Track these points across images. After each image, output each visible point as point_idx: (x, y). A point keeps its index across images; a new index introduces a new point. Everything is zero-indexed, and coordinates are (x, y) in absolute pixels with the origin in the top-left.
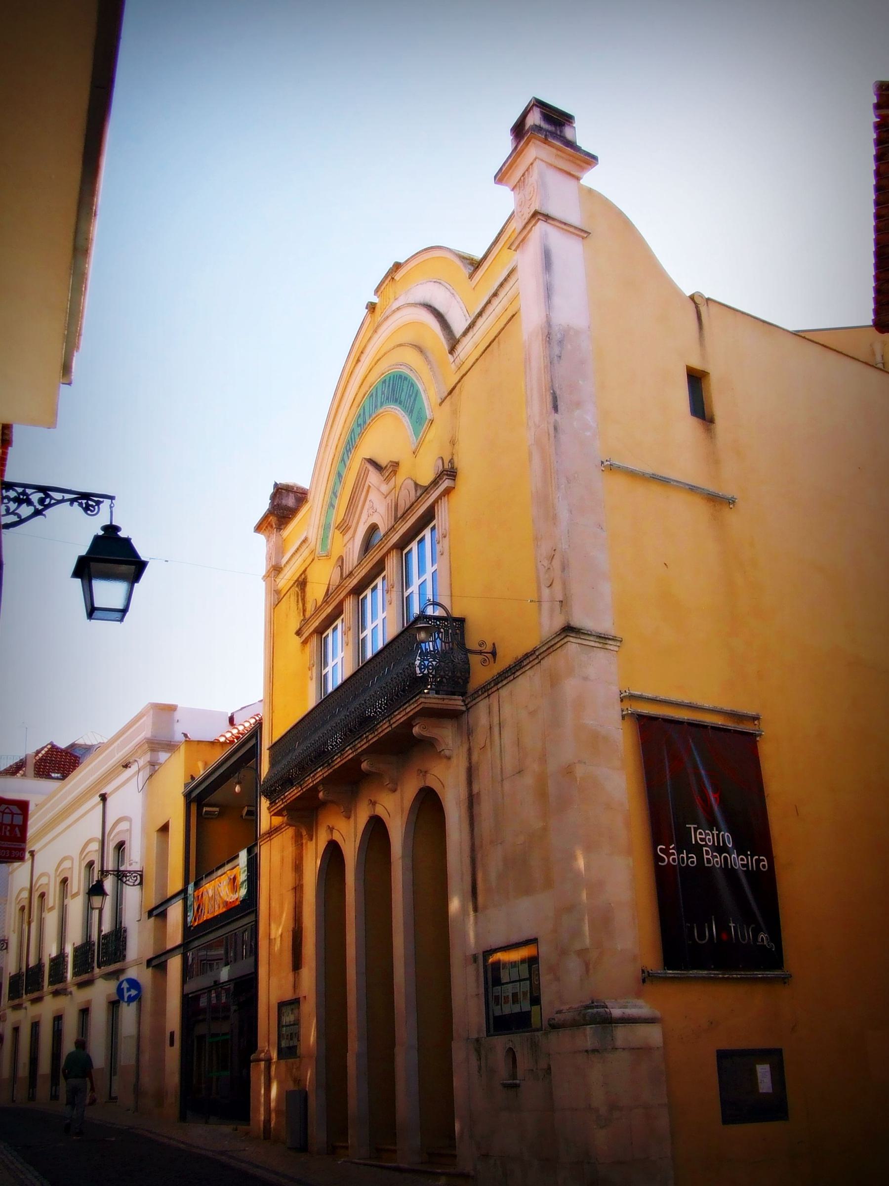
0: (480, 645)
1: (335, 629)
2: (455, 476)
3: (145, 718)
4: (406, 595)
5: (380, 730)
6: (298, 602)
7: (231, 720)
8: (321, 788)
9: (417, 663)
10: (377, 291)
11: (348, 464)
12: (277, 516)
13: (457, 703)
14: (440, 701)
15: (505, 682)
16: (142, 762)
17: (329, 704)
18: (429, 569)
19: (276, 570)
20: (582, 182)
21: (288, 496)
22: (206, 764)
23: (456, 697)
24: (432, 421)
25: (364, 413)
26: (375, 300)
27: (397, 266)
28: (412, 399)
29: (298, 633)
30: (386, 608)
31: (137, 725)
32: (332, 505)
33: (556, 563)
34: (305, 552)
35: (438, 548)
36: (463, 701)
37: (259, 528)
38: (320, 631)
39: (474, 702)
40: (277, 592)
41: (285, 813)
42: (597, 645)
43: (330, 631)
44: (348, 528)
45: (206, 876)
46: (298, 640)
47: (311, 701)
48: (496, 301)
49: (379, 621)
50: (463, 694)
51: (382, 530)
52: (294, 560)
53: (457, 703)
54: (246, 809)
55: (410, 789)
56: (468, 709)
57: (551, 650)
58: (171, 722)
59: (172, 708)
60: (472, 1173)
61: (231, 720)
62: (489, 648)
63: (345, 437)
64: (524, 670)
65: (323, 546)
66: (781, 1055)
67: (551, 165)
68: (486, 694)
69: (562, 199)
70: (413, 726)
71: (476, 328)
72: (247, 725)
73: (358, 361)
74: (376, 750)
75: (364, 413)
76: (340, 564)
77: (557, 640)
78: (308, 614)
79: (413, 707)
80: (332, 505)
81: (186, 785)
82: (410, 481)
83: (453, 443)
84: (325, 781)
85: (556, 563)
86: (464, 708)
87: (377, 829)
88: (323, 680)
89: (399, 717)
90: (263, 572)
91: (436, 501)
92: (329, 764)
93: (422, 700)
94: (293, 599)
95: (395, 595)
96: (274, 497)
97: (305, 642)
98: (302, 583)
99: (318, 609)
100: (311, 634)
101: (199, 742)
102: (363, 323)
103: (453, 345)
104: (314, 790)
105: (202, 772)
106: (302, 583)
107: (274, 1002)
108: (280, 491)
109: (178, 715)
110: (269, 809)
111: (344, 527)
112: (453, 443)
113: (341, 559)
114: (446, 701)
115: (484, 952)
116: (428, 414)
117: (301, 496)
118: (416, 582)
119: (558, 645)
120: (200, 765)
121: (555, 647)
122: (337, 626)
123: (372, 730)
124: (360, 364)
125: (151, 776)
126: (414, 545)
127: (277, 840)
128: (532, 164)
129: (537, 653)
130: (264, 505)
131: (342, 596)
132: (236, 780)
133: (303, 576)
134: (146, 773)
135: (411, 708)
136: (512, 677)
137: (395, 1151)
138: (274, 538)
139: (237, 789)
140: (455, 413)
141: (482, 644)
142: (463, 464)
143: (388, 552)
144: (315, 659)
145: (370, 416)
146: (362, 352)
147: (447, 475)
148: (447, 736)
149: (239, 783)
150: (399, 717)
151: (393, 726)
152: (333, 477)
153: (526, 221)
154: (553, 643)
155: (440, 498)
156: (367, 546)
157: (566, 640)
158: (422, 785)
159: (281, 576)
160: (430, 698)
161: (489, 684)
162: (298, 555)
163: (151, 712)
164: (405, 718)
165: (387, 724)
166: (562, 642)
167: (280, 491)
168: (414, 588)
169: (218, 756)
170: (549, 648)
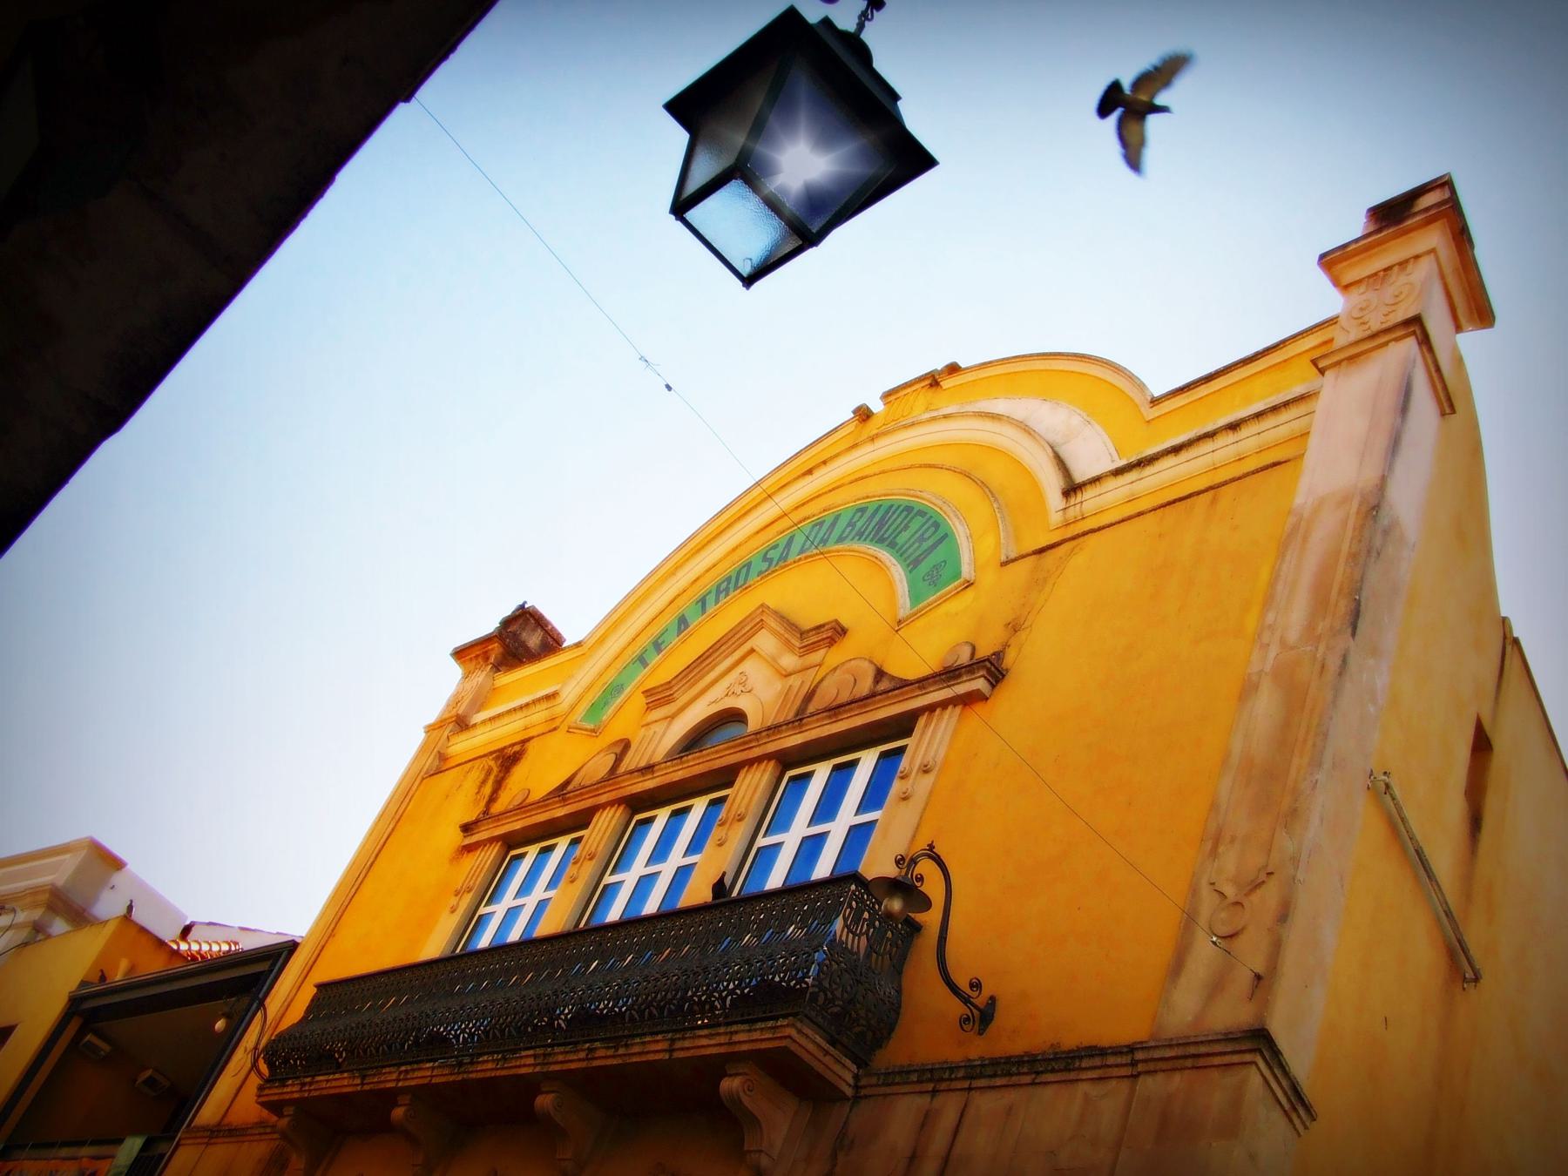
0: (972, 986)
2: (998, 681)
3: (67, 856)
4: (762, 841)
5: (636, 1049)
6: (484, 782)
7: (186, 931)
8: (406, 1099)
10: (887, 396)
11: (711, 609)
12: (506, 647)
13: (843, 1073)
14: (820, 1055)
15: (998, 1082)
16: (22, 917)
17: (460, 964)
18: (539, 892)
19: (460, 723)
20: (1459, 336)
21: (534, 630)
22: (132, 968)
23: (848, 1063)
24: (969, 584)
25: (833, 524)
26: (877, 406)
27: (953, 369)
28: (926, 545)
29: (467, 828)
30: (562, 884)
31: (54, 859)
32: (642, 660)
33: (1269, 896)
34: (538, 716)
35: (571, 870)
36: (856, 1077)
37: (460, 654)
38: (512, 843)
39: (888, 1090)
40: (443, 757)
41: (289, 1110)
42: (1284, 1101)
44: (668, 700)
45: (35, 1146)
46: (455, 838)
47: (433, 947)
48: (1170, 461)
50: (861, 1063)
51: (754, 724)
52: (506, 720)
53: (843, 1073)
54: (149, 1073)
56: (857, 1098)
57: (1189, 1063)
58: (102, 883)
59: (117, 864)
61: (186, 931)
62: (980, 1001)
63: (727, 568)
64: (1072, 1076)
65: (561, 732)
67: (1442, 277)
68: (930, 1086)
70: (725, 1075)
71: (1149, 470)
72: (215, 948)
73: (810, 472)
74: (586, 1084)
75: (833, 524)
76: (618, 750)
77: (1218, 1048)
78: (497, 808)
79: (756, 1035)
80: (642, 660)
81: (83, 984)
82: (866, 664)
83: (1014, 627)
84: (426, 1094)
85: (1269, 896)
86: (849, 1092)
88: (474, 922)
89: (705, 1042)
90: (432, 716)
91: (931, 708)
92: (460, 1064)
93: (792, 1032)
94: (476, 775)
95: (588, 870)
96: (507, 623)
97: (468, 849)
98: (508, 759)
99: (522, 808)
100: (492, 840)
101: (143, 930)
102: (835, 430)
103: (1072, 489)
104: (389, 1097)
105: (118, 977)
106: (508, 759)
108: (525, 617)
109: (118, 879)
110: (261, 1088)
111: (658, 697)
112: (1014, 627)
113: (626, 745)
114: (827, 1059)
116: (966, 571)
117: (552, 643)
118: (508, 900)
119: (1217, 1061)
120: (124, 965)
121: (1202, 1062)
123: (615, 1042)
124: (809, 478)
125: (25, 944)
126: (532, 851)
128: (1417, 257)
129: (1139, 1055)
130: (488, 624)
131: (603, 799)
132: (226, 1009)
133: (517, 748)
134: (23, 935)
135: (747, 1038)
136: (1028, 1079)
138: (481, 677)
139: (220, 1025)
140: (1038, 583)
142: (1026, 662)
143: (759, 760)
144: (480, 880)
145: (802, 551)
146: (824, 462)
147: (989, 670)
149: (228, 1016)
150: (705, 1042)
151: (677, 1055)
152: (669, 619)
153: (1389, 324)
154: (1203, 1049)
155: (944, 705)
156: (695, 740)
157: (1248, 1057)
159: (463, 736)
160: (804, 1039)
161: (952, 1069)
162: (520, 715)
163: (83, 853)
164: (722, 1050)
165: (664, 1045)
166: (1235, 1058)
167: (525, 617)
168: (499, 910)
169: (154, 965)
170: (1186, 1057)
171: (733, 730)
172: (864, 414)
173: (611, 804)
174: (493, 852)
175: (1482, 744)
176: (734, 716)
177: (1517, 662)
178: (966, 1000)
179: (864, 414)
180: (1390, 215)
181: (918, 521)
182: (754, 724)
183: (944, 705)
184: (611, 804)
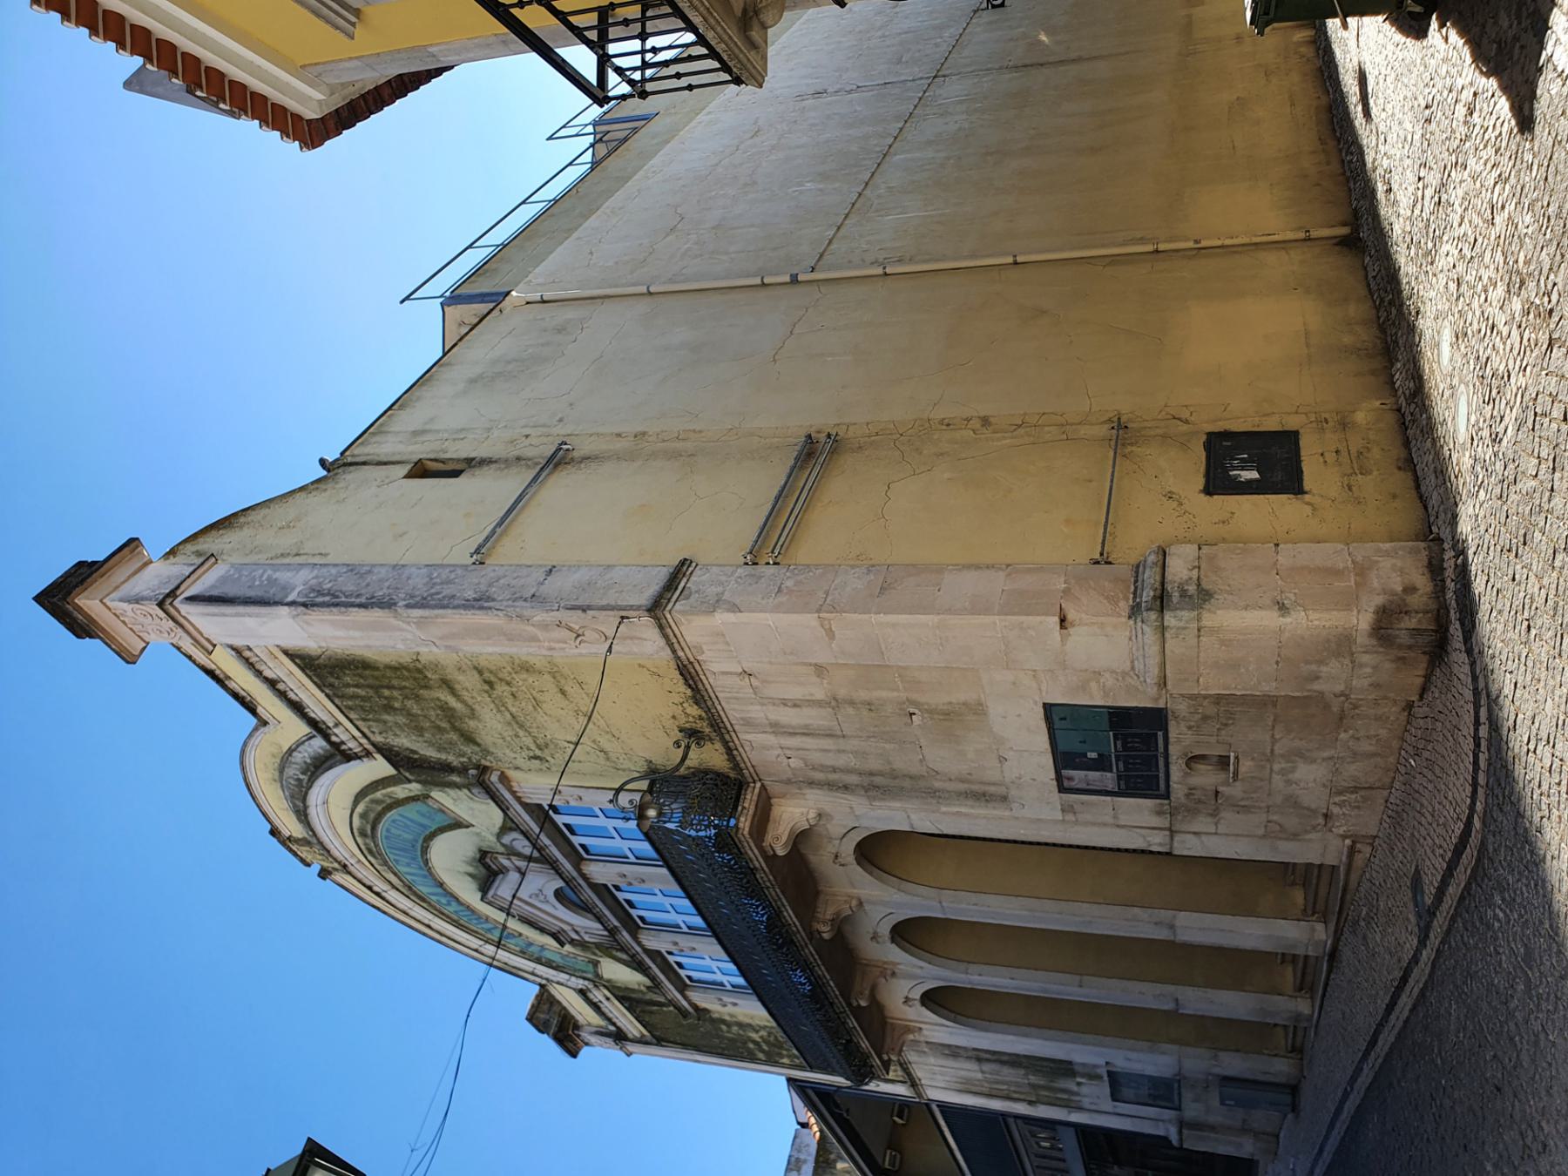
1: (680, 965)
4: (633, 859)
9: (693, 833)
19: (619, 1037)
26: (316, 868)
34: (598, 995)
37: (574, 1055)
43: (682, 973)
49: (714, 965)
51: (559, 883)
55: (895, 954)
60: (1348, 842)
66: (1226, 435)
69: (157, 575)
70: (775, 855)
87: (908, 933)
91: (518, 799)
100: (685, 997)
107: (1108, 1105)
115: (1062, 789)
118: (719, 977)
122: (567, 826)
127: (919, 1072)
130: (546, 1043)
131: (638, 949)
137: (1306, 957)
141: (677, 744)
148: (792, 814)
158: (917, 1003)
168: (724, 979)
171: (568, 892)
172: (324, 874)
173: (639, 944)
174: (692, 995)
175: (420, 471)
176: (558, 894)
177: (356, 450)
178: (688, 747)
179: (324, 874)
180: (81, 627)
181: (393, 830)
182: (559, 883)
183: (513, 793)
184: (639, 944)
